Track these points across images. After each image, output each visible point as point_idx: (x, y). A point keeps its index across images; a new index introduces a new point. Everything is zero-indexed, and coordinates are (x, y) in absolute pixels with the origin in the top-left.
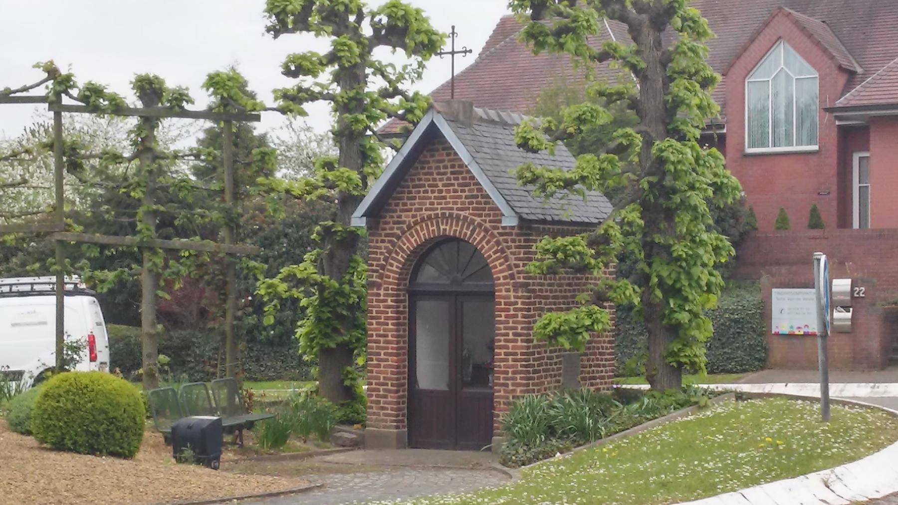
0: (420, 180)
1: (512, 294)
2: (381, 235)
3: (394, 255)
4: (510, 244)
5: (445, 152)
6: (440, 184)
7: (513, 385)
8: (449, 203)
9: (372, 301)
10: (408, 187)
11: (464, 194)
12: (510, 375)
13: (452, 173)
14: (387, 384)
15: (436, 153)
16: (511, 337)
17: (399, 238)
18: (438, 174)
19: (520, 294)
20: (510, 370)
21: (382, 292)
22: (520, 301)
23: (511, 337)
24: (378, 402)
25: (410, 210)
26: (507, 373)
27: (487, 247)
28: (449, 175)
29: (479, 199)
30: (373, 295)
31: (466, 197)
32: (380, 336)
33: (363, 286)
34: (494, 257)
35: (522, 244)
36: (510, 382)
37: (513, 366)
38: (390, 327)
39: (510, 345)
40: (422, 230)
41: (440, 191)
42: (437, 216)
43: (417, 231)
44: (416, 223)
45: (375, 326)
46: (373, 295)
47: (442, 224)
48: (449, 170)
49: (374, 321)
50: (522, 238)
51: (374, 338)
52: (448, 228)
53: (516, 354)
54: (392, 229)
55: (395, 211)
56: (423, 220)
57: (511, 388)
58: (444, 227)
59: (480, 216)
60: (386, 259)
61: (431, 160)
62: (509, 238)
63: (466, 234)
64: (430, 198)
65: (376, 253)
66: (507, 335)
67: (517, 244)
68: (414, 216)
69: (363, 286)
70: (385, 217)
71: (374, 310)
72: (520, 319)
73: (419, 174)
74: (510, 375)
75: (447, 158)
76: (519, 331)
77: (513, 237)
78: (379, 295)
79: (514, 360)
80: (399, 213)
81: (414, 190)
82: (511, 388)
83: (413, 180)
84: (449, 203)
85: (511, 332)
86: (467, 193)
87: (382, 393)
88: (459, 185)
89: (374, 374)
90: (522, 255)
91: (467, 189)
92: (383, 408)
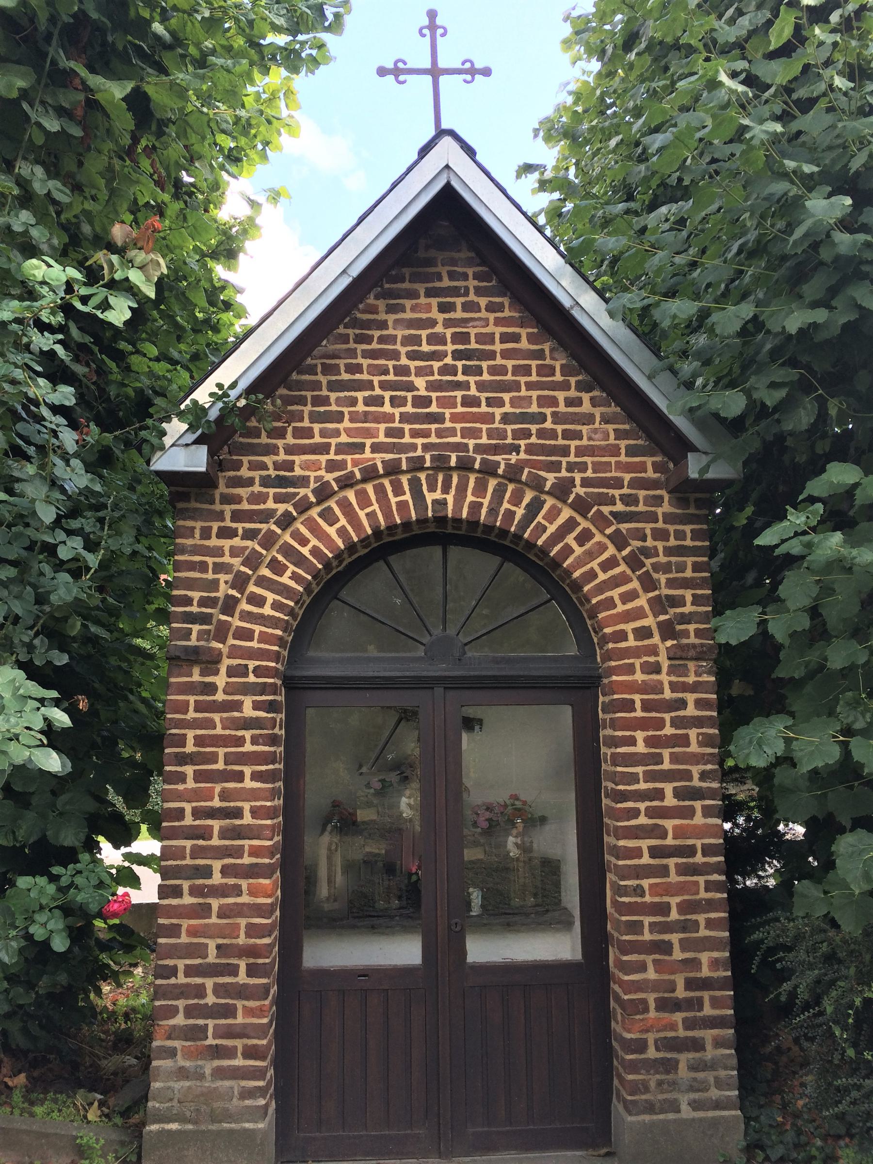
0: (358, 369)
1: (664, 678)
2: (220, 516)
3: (265, 572)
4: (650, 543)
5: (434, 302)
6: (420, 383)
7: (685, 945)
8: (452, 432)
9: (183, 708)
10: (317, 386)
11: (498, 412)
12: (674, 915)
13: (458, 355)
14: (233, 971)
15: (408, 303)
16: (670, 801)
17: (286, 521)
18: (412, 356)
19: (691, 679)
20: (674, 901)
21: (221, 680)
22: (691, 698)
23: (670, 801)
24: (195, 1033)
25: (324, 449)
26: (664, 909)
27: (578, 550)
28: (449, 360)
29: (548, 425)
30: (190, 688)
31: (506, 419)
32: (212, 813)
33: (796, 987)
34: (602, 577)
35: (688, 542)
36: (674, 938)
37: (680, 889)
38: (249, 783)
39: (669, 824)
40: (364, 502)
41: (424, 402)
42: (417, 465)
43: (345, 505)
44: (346, 483)
45: (190, 784)
46: (190, 688)
47: (432, 489)
48: (450, 347)
49: (189, 770)
50: (688, 528)
51: (188, 820)
52: (450, 499)
53: (690, 851)
54: (261, 498)
55: (271, 450)
56: (370, 474)
57: (678, 954)
58: (438, 495)
59: (555, 467)
60: (240, 582)
61: (391, 318)
62: (648, 527)
63: (510, 514)
64: (390, 418)
65: (203, 567)
66: (659, 794)
67: (672, 542)
68: (332, 466)
69: (796, 987)
70: (238, 466)
71: (190, 734)
72: (694, 748)
73: (352, 353)
74: (674, 915)
75: (440, 317)
76: (696, 782)
77: (660, 525)
78: (211, 688)
79: (683, 870)
80: (282, 456)
81: (333, 396)
82: (678, 954)
83: (328, 370)
84: (452, 432)
85: (669, 788)
86: (507, 409)
87: (211, 999)
88: (482, 386)
89: (184, 939)
90: (689, 573)
91: (506, 397)
92: (217, 1052)
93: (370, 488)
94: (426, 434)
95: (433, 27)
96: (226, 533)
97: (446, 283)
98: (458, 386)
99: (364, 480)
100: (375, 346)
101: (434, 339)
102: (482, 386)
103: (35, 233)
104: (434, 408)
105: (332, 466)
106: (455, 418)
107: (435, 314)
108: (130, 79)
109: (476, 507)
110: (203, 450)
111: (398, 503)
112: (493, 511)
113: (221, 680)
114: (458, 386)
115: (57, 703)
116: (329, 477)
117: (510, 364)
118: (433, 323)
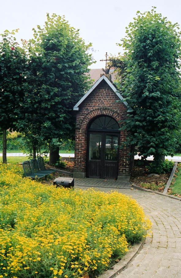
21: (80, 131)
25: (91, 106)
31: (111, 103)
64: (98, 103)
93: (96, 111)
94: (102, 105)
95: (106, 55)
96: (81, 115)
97: (101, 91)
98: (106, 99)
99: (95, 110)
100: (97, 95)
101: (104, 94)
102: (108, 99)
103: (62, 98)
104: (103, 102)
105: (92, 108)
106: (106, 103)
107: (104, 91)
108: (64, 120)
109: (107, 113)
110: (78, 108)
111: (99, 113)
112: (109, 114)
113: (80, 131)
114: (106, 99)
115: (153, 112)
116: (92, 110)
117: (112, 97)
118: (103, 92)
